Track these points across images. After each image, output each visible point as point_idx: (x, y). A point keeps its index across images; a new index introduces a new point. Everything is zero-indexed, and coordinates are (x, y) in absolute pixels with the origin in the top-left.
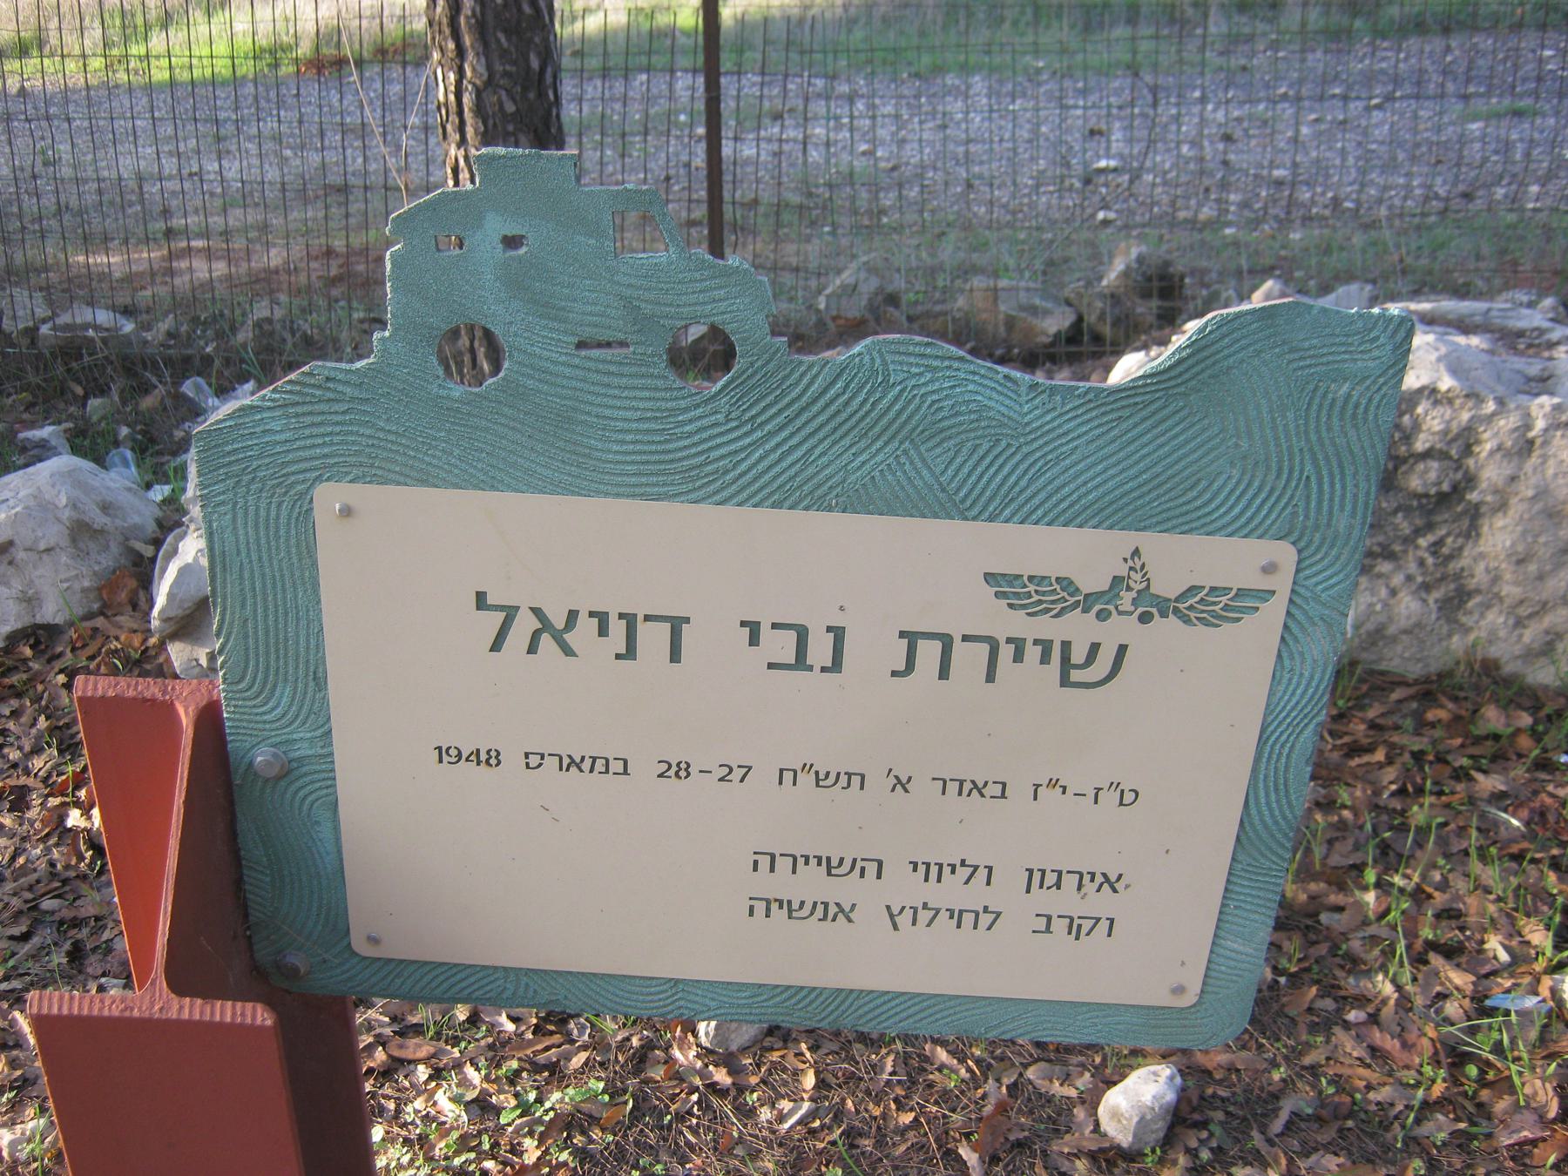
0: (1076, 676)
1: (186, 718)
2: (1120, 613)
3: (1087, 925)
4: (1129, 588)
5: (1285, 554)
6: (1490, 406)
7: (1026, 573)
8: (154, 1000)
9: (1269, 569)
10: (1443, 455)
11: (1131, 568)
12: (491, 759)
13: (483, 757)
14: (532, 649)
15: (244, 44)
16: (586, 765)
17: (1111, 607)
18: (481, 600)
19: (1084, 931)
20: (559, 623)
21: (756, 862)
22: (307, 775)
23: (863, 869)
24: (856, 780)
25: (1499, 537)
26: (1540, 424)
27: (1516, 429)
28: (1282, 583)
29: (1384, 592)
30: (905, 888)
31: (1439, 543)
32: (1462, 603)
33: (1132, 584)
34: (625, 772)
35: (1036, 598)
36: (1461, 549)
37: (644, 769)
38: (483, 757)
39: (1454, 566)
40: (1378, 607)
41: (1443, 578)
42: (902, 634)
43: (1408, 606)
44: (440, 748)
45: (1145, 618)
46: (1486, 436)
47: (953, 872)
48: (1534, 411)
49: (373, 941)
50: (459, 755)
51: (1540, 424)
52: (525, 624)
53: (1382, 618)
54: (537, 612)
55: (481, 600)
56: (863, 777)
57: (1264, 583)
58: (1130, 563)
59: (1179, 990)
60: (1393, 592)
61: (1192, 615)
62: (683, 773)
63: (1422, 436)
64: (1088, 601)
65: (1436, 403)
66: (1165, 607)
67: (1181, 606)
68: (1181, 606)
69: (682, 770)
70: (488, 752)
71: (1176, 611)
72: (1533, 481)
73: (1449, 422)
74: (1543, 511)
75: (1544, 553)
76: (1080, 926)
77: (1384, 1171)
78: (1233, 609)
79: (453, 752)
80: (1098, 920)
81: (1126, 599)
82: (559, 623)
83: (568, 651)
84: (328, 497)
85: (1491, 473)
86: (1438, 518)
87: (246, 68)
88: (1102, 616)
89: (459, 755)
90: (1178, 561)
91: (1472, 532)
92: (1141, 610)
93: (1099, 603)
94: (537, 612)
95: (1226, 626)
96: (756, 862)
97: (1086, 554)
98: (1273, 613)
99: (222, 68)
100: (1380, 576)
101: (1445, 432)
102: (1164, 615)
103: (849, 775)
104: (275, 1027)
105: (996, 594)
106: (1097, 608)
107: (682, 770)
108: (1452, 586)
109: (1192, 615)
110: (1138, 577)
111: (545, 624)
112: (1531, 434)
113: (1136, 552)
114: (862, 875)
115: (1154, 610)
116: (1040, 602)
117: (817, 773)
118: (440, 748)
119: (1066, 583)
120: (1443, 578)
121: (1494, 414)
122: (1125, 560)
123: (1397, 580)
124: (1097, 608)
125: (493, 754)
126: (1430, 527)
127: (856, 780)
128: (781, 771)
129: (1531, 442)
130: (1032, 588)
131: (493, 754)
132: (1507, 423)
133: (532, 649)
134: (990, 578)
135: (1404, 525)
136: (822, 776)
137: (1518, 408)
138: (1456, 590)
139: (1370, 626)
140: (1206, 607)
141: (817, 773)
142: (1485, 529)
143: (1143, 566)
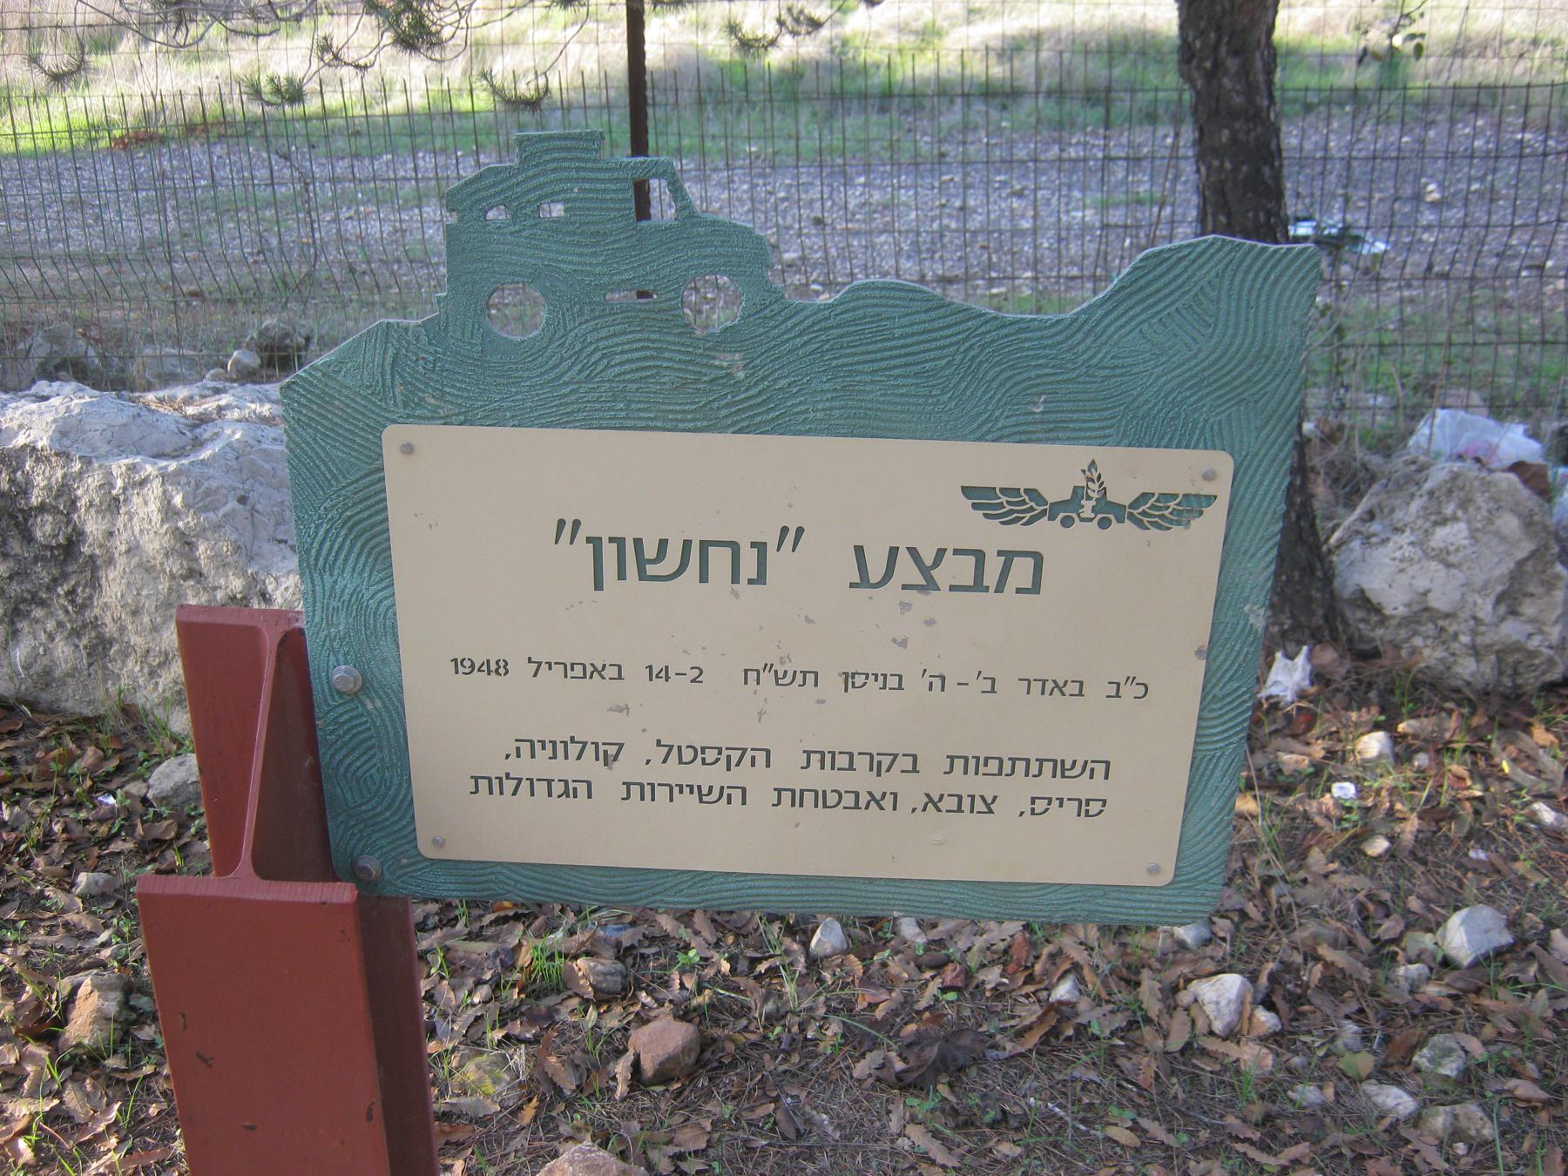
0: (651, 570)
2: (1083, 520)
4: (1089, 498)
5: (1223, 463)
6: (77, 466)
7: (998, 485)
8: (245, 884)
9: (1209, 477)
10: (54, 510)
12: (499, 668)
13: (493, 667)
15: (79, 120)
16: (589, 669)
19: (734, 761)
21: (518, 749)
24: (810, 677)
25: (114, 587)
26: (119, 483)
27: (101, 486)
29: (43, 637)
30: (759, 782)
31: (72, 593)
32: (106, 650)
34: (900, 687)
35: (1008, 508)
36: (90, 598)
38: (493, 667)
39: (89, 615)
40: (41, 651)
41: (84, 626)
43: (63, 652)
45: (1105, 524)
46: (79, 492)
48: (115, 471)
49: (438, 843)
50: (473, 666)
51: (119, 483)
53: (46, 661)
56: (816, 674)
57: (1207, 489)
59: (1154, 870)
60: (51, 638)
63: (36, 491)
64: (1053, 511)
65: (38, 460)
66: (1119, 512)
71: (1132, 517)
72: (125, 536)
73: (49, 479)
74: (140, 565)
75: (150, 605)
76: (880, 763)
77: (459, 1165)
80: (744, 750)
81: (1088, 506)
85: (93, 527)
86: (70, 569)
87: (64, 144)
88: (1067, 522)
89: (473, 666)
90: (1134, 471)
91: (95, 583)
93: (1064, 511)
96: (518, 749)
97: (1051, 467)
98: (1216, 515)
99: (44, 143)
100: (37, 621)
101: (49, 488)
103: (804, 673)
106: (1061, 515)
108: (93, 634)
110: (1095, 486)
112: (114, 492)
114: (753, 765)
116: (1011, 512)
118: (455, 660)
119: (1033, 493)
120: (84, 626)
121: (81, 473)
123: (51, 625)
124: (1061, 515)
126: (65, 576)
127: (810, 677)
128: (746, 671)
129: (116, 499)
130: (1004, 499)
132: (94, 480)
134: (967, 491)
135: (43, 574)
137: (100, 467)
138: (97, 637)
139: (38, 668)
140: (1162, 512)
142: (103, 581)
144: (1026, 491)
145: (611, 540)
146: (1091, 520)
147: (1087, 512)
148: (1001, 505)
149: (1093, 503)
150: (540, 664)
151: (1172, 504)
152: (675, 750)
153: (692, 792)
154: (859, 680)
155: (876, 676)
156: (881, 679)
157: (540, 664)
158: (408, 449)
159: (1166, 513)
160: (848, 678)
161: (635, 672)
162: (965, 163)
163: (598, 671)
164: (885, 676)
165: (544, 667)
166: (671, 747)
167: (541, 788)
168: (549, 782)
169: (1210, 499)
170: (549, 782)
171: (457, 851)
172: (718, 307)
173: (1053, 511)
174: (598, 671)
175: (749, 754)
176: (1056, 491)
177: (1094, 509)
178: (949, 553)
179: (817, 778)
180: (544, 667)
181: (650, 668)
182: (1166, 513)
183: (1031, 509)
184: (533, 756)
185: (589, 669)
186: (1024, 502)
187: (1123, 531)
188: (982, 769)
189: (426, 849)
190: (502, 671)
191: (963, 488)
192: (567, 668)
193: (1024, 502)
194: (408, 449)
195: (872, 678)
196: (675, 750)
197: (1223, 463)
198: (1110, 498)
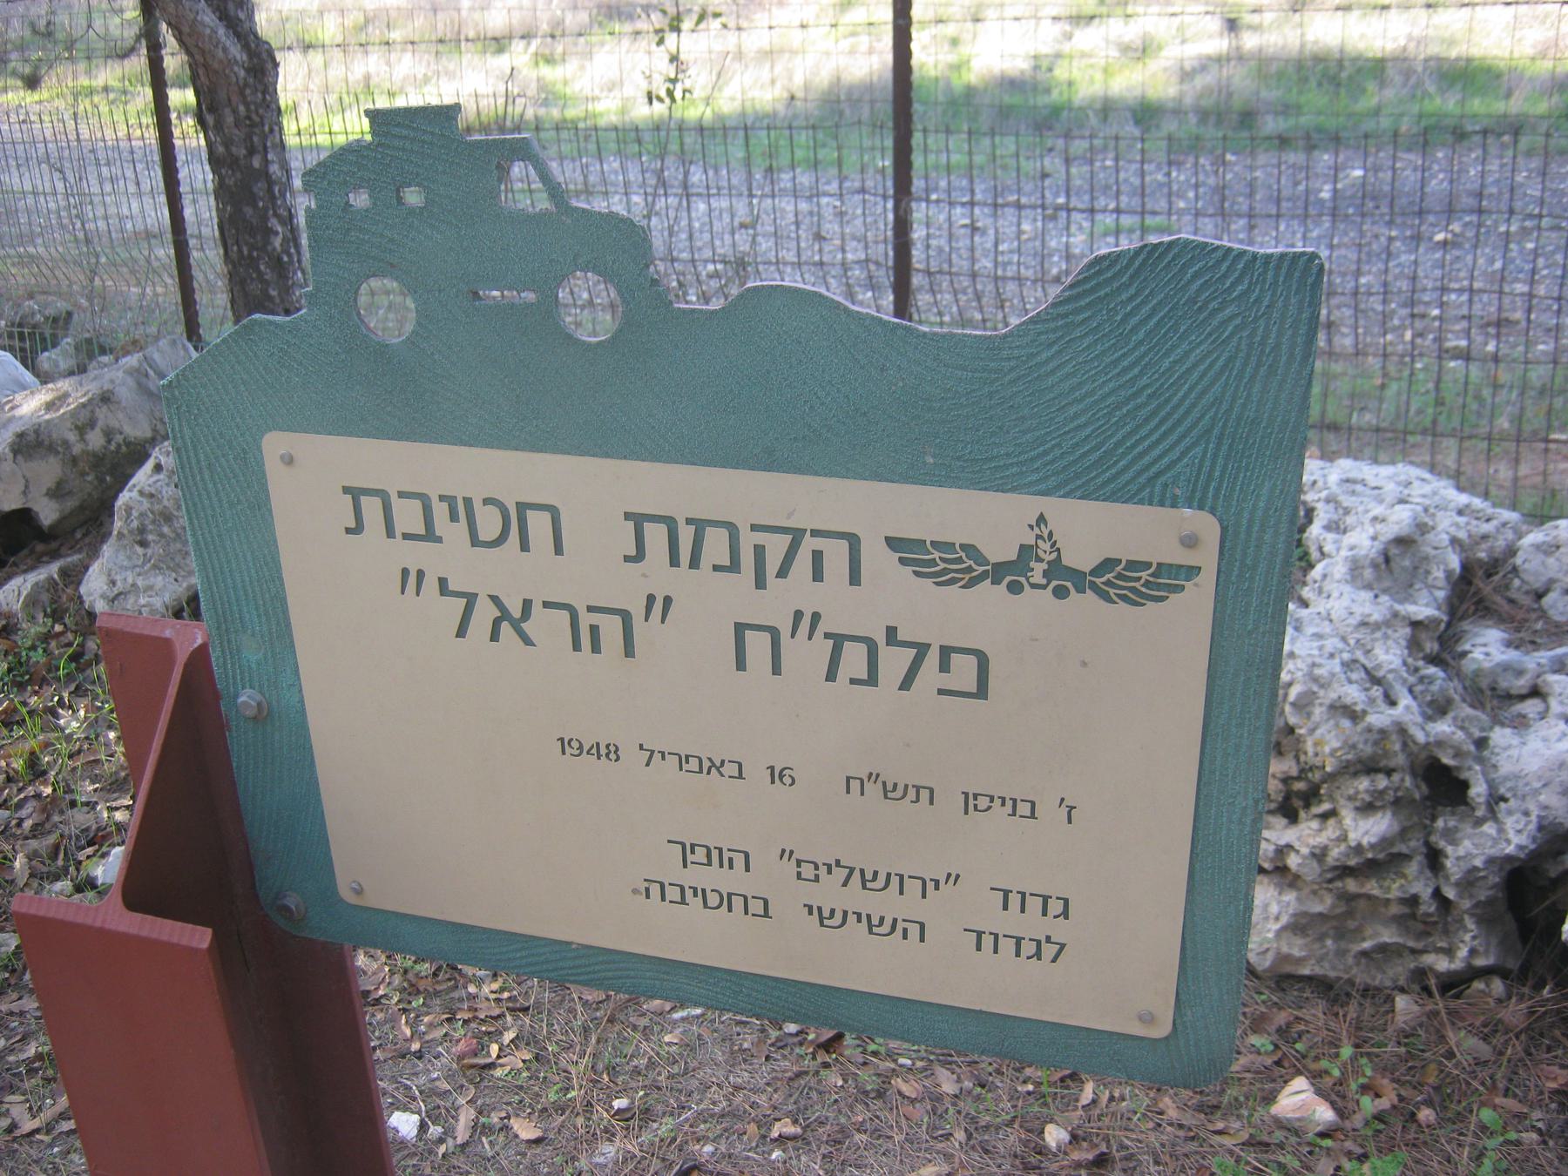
1: (182, 657)
2: (1033, 586)
3: (776, 547)
5: (1206, 526)
9: (1190, 542)
11: (1038, 537)
13: (603, 751)
14: (495, 636)
16: (706, 764)
17: (1022, 579)
18: (641, 746)
19: (773, 564)
20: (516, 613)
21: (647, 890)
22: (285, 727)
23: (817, 556)
24: (925, 794)
28: (1207, 558)
33: (1041, 553)
34: (1033, 816)
35: (943, 565)
37: (757, 772)
38: (603, 751)
42: (346, 490)
44: (562, 740)
47: (829, 872)
50: (581, 747)
52: (484, 614)
54: (495, 599)
55: (641, 746)
58: (1037, 530)
61: (1112, 591)
62: (612, 756)
64: (998, 572)
67: (1098, 581)
68: (1098, 581)
69: (777, 775)
70: (608, 746)
71: (1095, 588)
78: (1159, 587)
79: (575, 744)
80: (797, 535)
81: (1037, 572)
82: (516, 613)
83: (528, 641)
84: (274, 444)
88: (1015, 588)
89: (581, 747)
90: (1090, 529)
92: (1054, 583)
93: (1010, 574)
94: (495, 599)
95: (1149, 603)
96: (647, 890)
97: (994, 520)
98: (1208, 579)
102: (1081, 590)
103: (918, 788)
104: (210, 949)
105: (900, 559)
106: (1008, 579)
107: (777, 775)
109: (1112, 591)
111: (505, 614)
113: (1041, 519)
115: (1068, 584)
117: (884, 784)
118: (562, 740)
122: (1031, 527)
124: (1008, 579)
125: (612, 748)
127: (925, 794)
130: (936, 555)
131: (612, 748)
133: (495, 636)
136: (889, 787)
141: (884, 784)
143: (1051, 534)
144: (961, 546)
145: (486, 501)
146: (1044, 587)
147: (1037, 578)
148: (933, 563)
149: (1045, 566)
150: (652, 752)
151: (1144, 575)
152: (857, 874)
153: (859, 921)
154: (983, 802)
155: (1003, 800)
156: (1009, 803)
157: (652, 752)
158: (289, 460)
159: (1137, 585)
160: (969, 801)
161: (757, 772)
162: (948, 168)
163: (717, 767)
164: (1015, 801)
165: (657, 756)
166: (852, 870)
167: (1007, 946)
168: (1046, 899)
169: (1198, 569)
170: (1046, 899)
171: (372, 900)
172: (589, 307)
173: (998, 572)
174: (717, 767)
175: (809, 544)
176: (1001, 551)
177: (1045, 574)
178: (537, 608)
179: (1011, 922)
180: (657, 756)
181: (772, 768)
182: (1137, 585)
183: (970, 569)
184: (924, 896)
185: (706, 764)
186: (959, 560)
187: (1084, 603)
188: (685, 766)
189: (346, 894)
190: (612, 756)
191: (887, 539)
192: (683, 760)
193: (959, 560)
194: (289, 460)
195: (998, 802)
196: (857, 874)
197: (1206, 526)
198: (1065, 562)
